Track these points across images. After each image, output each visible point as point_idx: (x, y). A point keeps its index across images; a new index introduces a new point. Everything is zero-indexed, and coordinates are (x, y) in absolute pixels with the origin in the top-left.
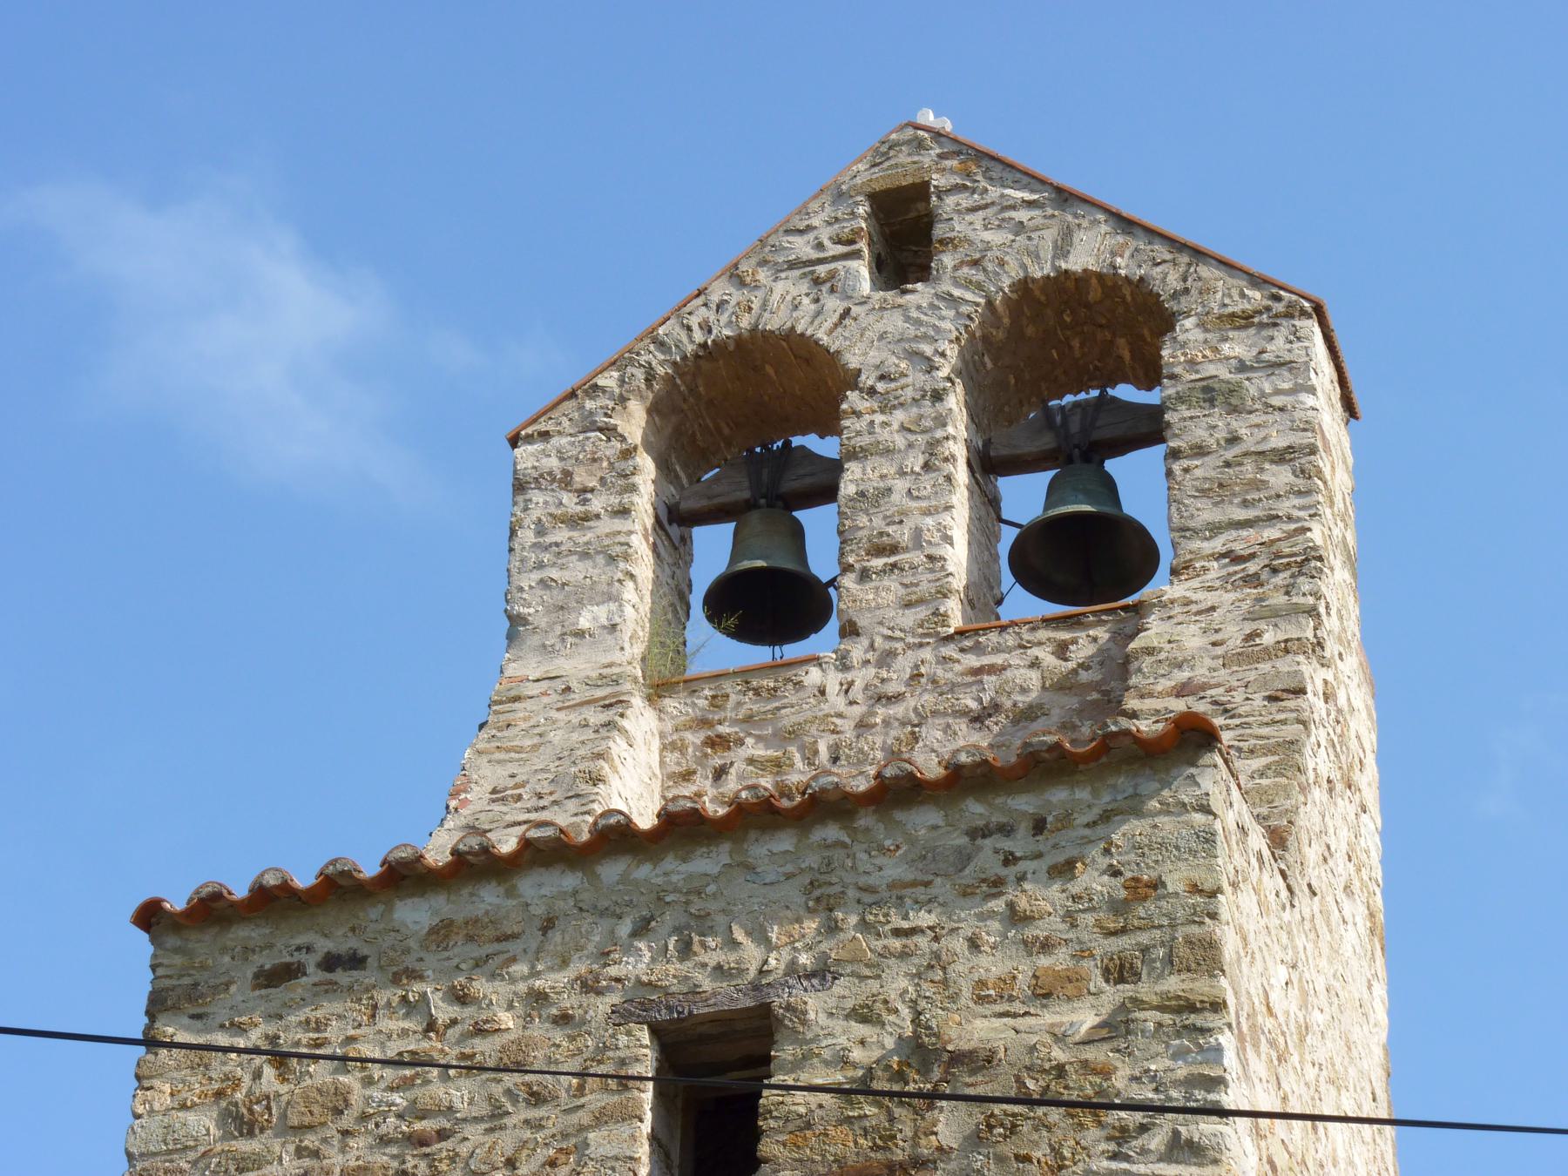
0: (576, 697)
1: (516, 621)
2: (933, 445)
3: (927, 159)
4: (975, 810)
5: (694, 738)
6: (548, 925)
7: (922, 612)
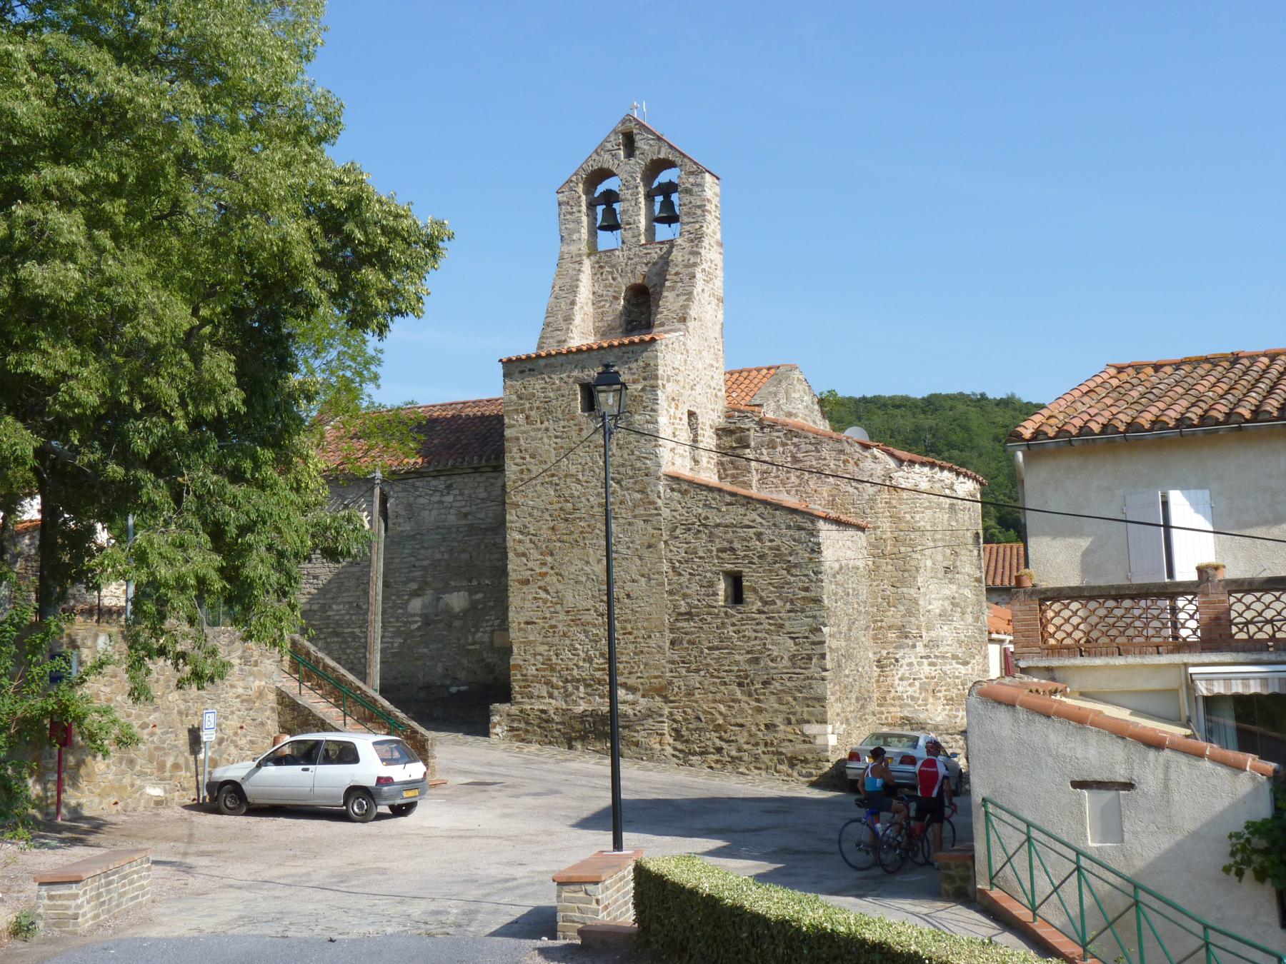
0: (574, 260)
1: (562, 237)
2: (637, 199)
3: (633, 125)
5: (597, 266)
7: (636, 239)
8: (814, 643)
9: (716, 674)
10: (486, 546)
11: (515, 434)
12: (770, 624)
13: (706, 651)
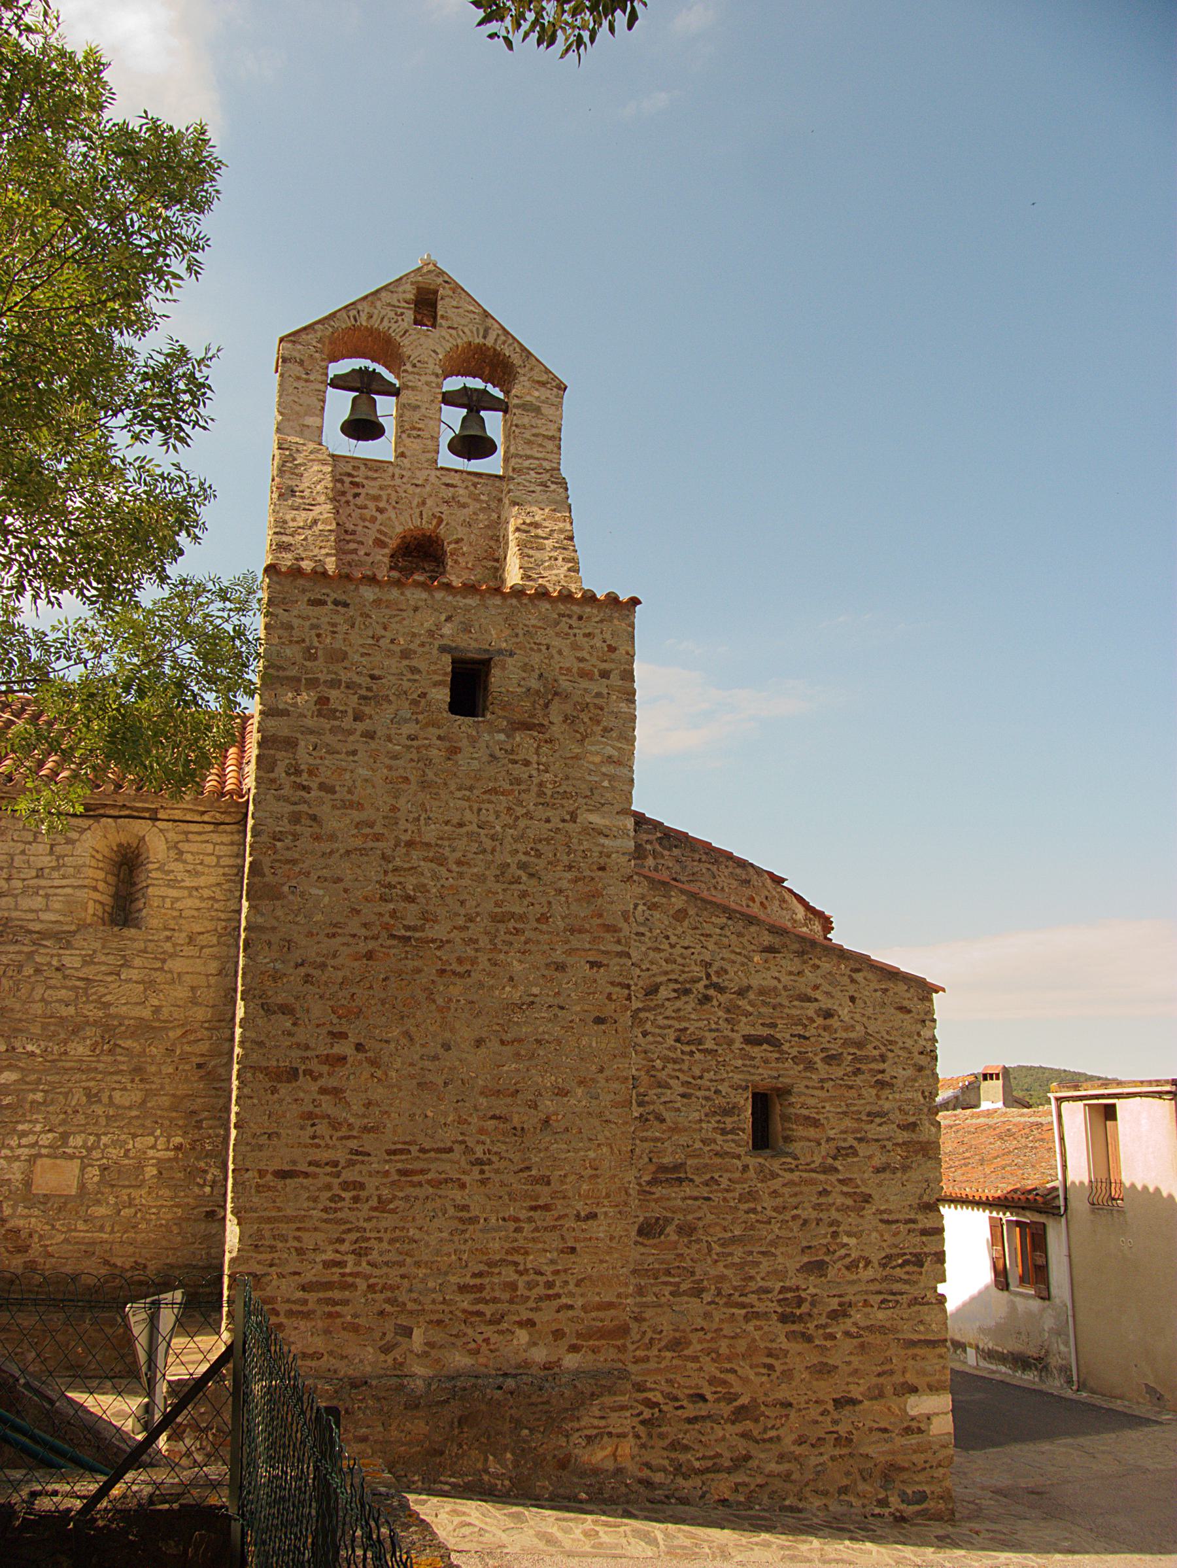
4: (561, 607)
6: (416, 609)
8: (924, 1232)
9: (736, 1298)
10: (38, 971)
11: (285, 732)
12: (845, 1194)
13: (717, 1248)
